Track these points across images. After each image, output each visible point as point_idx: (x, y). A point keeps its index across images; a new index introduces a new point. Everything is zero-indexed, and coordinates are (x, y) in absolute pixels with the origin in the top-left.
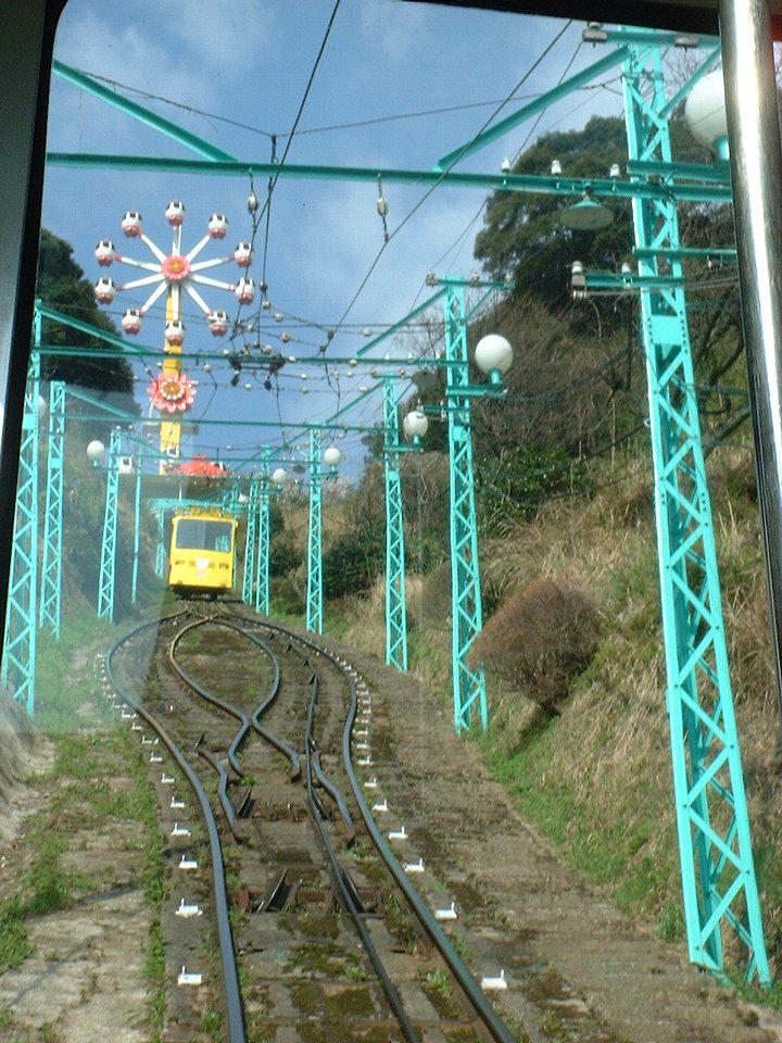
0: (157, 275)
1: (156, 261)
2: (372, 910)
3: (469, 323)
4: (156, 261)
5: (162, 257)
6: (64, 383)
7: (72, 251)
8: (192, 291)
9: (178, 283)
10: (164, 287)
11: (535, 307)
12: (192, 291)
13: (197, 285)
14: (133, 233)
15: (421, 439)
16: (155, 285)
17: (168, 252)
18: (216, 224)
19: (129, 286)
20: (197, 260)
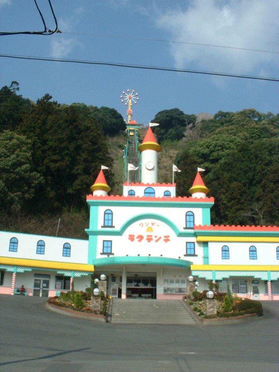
0: (128, 97)
1: (133, 97)
2: (253, 116)
3: (183, 278)
4: (133, 97)
5: (128, 96)
6: (65, 275)
7: (46, 94)
8: (132, 99)
9: (130, 98)
10: (129, 99)
11: (224, 309)
12: (132, 99)
13: (132, 98)
14: (124, 94)
15: (272, 118)
16: (127, 99)
17: (128, 95)
18: (133, 91)
19: (125, 100)
20: (131, 95)
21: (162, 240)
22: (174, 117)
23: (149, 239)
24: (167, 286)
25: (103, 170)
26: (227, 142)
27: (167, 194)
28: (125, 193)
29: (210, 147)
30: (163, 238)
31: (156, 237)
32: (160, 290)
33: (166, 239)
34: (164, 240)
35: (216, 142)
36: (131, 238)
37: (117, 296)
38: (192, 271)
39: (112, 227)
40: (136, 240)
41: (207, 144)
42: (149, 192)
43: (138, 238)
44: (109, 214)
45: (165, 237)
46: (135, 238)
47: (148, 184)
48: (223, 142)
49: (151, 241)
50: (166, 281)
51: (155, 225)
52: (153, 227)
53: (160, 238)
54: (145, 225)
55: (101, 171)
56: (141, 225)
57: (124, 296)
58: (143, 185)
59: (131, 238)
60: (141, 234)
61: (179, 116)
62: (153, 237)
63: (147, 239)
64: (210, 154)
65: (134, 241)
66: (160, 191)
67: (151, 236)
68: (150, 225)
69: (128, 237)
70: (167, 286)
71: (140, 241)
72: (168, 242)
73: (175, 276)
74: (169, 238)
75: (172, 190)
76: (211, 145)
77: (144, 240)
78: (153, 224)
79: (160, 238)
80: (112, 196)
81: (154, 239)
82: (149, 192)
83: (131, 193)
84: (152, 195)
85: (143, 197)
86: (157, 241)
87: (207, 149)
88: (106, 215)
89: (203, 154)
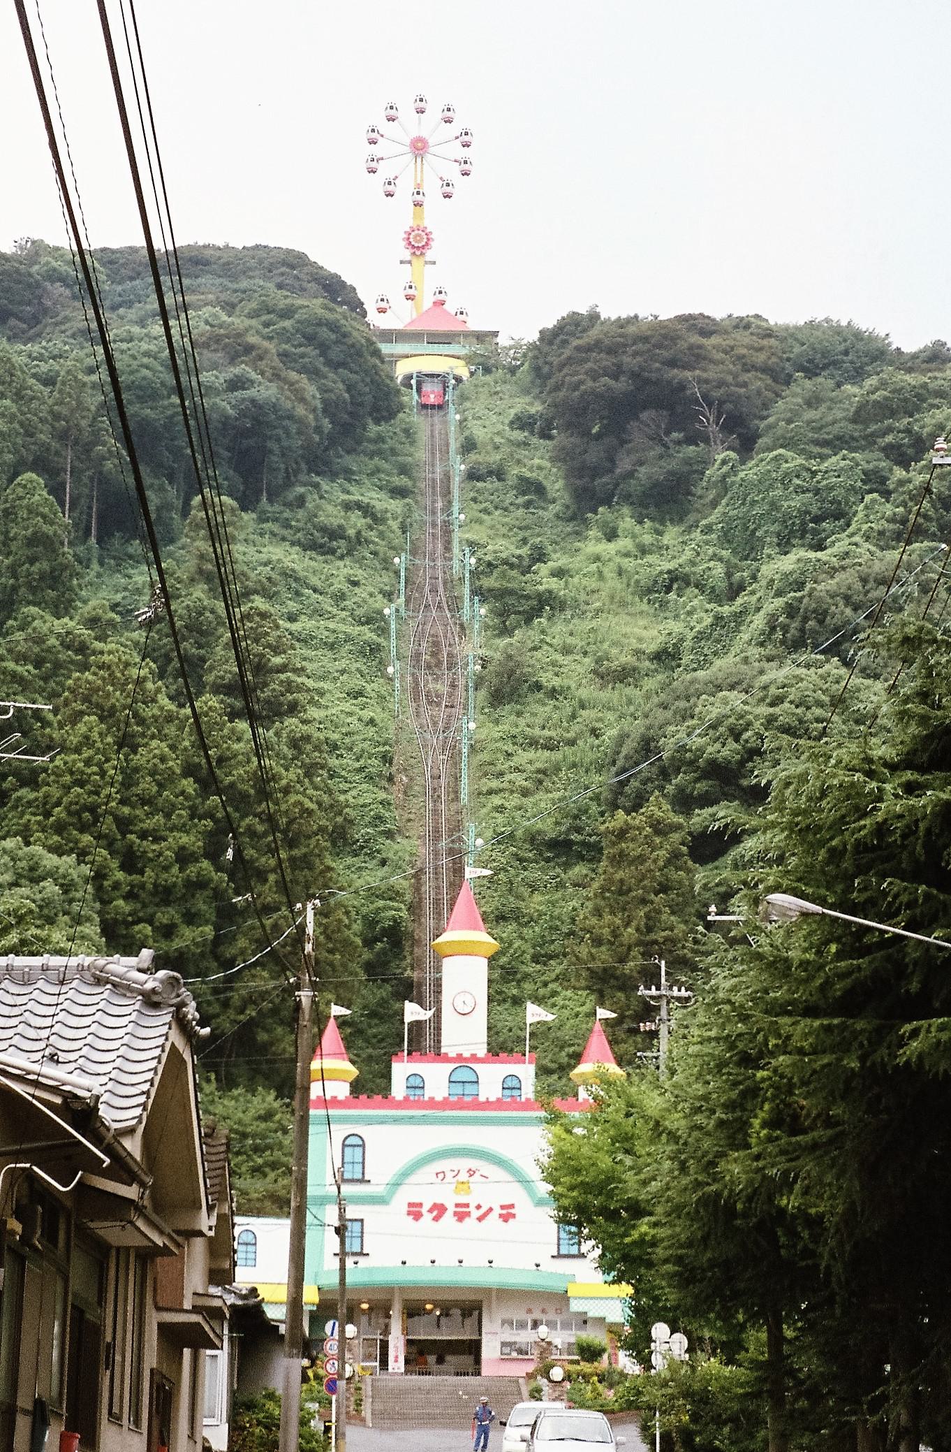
21: (494, 1216)
22: (654, 376)
23: (461, 1217)
24: (509, 1335)
25: (336, 1018)
26: (818, 712)
27: (511, 1085)
28: (398, 1089)
29: (745, 736)
30: (497, 1211)
31: (479, 1207)
32: (490, 1350)
33: (504, 1212)
34: (501, 1216)
35: (771, 710)
36: (415, 1211)
37: (377, 1364)
38: (571, 1300)
39: (363, 1181)
40: (427, 1217)
41: (732, 720)
42: (464, 1083)
43: (430, 1211)
44: (354, 1144)
45: (502, 1207)
46: (424, 1210)
47: (459, 1058)
48: (799, 711)
49: (467, 1220)
50: (508, 1322)
51: (477, 1177)
52: (471, 1179)
53: (491, 1209)
54: (449, 1175)
55: (332, 1020)
56: (441, 1176)
57: (397, 1363)
58: (447, 1059)
59: (415, 1211)
60: (439, 1201)
61: (676, 374)
62: (472, 1209)
63: (455, 1214)
64: (742, 763)
65: (422, 1220)
66: (491, 1079)
67: (467, 1205)
68: (463, 1176)
69: (405, 1208)
70: (509, 1335)
71: (436, 1219)
72: (511, 1221)
73: (529, 1311)
74: (512, 1211)
75: (526, 1072)
76: (749, 724)
77: (449, 1217)
78: (471, 1173)
79: (491, 1209)
80: (363, 1097)
81: (476, 1214)
82: (464, 1083)
83: (416, 1084)
84: (469, 1089)
85: (445, 1099)
86: (480, 1219)
87: (732, 745)
88: (347, 1149)
89: (713, 763)
